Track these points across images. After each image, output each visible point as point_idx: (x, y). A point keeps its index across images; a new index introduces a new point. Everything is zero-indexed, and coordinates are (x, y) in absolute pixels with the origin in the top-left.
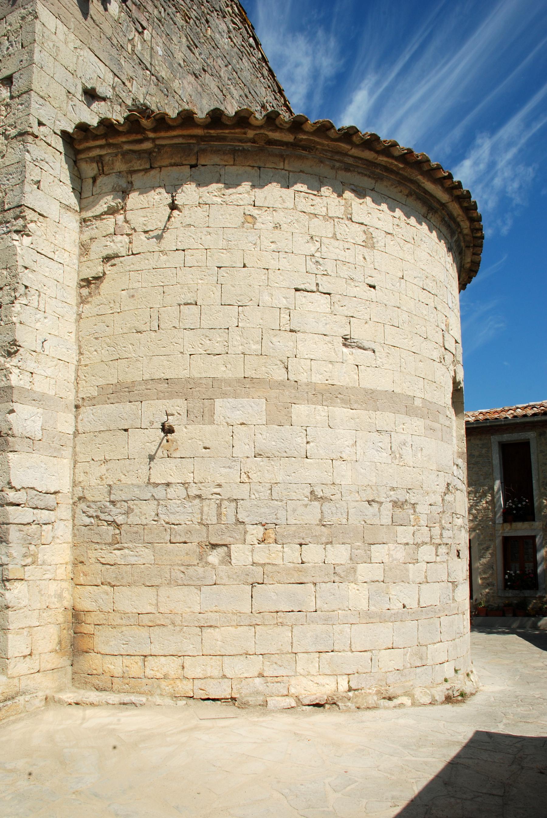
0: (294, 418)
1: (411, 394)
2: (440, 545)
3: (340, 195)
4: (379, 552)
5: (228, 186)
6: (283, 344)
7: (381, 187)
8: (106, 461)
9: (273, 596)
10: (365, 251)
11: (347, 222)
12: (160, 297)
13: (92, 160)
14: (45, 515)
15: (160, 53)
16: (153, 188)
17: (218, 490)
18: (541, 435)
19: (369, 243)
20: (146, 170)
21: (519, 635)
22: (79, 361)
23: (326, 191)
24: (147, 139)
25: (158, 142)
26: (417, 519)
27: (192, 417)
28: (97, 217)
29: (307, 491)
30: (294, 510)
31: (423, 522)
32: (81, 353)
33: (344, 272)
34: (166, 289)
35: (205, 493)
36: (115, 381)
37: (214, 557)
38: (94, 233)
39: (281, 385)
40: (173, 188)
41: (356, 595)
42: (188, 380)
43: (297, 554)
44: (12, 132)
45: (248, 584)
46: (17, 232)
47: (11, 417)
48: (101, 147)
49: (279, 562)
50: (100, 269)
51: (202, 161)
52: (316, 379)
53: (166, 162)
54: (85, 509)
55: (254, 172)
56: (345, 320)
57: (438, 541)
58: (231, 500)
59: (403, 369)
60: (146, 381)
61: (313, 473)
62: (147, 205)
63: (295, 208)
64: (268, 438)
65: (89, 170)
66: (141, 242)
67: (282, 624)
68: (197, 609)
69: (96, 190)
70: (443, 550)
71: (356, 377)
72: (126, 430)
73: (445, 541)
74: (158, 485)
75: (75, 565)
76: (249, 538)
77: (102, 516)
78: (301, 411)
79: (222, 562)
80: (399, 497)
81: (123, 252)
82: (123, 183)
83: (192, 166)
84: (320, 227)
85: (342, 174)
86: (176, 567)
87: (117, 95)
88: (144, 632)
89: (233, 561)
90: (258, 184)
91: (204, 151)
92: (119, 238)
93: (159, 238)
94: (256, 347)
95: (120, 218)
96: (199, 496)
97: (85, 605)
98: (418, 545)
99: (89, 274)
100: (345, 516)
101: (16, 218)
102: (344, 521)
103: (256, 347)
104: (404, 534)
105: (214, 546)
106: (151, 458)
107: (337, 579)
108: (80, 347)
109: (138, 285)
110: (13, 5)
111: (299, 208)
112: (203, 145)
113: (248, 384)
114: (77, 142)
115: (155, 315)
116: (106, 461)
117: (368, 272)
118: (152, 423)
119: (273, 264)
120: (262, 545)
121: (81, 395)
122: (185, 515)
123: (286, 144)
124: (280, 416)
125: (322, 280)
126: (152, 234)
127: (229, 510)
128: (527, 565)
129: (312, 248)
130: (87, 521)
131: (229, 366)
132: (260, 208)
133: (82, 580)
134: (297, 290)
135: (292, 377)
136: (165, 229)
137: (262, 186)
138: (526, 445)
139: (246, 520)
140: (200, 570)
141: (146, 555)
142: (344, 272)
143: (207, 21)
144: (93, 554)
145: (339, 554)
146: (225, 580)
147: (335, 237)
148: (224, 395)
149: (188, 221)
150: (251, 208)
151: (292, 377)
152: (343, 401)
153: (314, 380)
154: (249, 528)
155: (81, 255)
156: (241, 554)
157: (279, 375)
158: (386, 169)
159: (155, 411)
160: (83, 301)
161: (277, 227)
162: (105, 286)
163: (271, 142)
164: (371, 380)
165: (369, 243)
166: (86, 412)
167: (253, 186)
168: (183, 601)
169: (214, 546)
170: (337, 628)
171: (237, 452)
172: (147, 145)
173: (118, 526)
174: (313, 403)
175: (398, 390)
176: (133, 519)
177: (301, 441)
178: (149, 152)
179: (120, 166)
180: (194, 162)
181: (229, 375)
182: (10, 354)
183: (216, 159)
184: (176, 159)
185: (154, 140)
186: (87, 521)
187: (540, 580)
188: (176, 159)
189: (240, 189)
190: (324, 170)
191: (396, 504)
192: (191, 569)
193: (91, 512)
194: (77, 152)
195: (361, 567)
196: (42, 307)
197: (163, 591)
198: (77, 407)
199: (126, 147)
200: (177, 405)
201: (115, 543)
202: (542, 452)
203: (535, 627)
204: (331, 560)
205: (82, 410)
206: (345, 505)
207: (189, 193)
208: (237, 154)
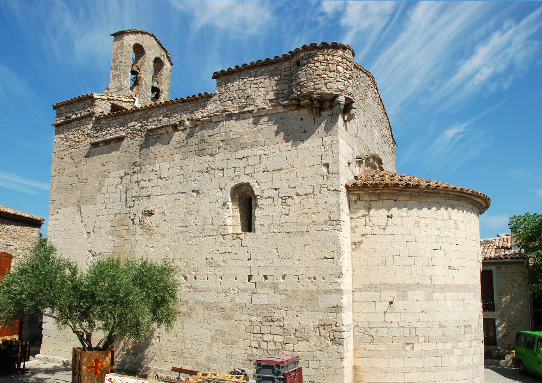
3: (447, 210)
4: (460, 344)
5: (409, 209)
7: (460, 203)
8: (367, 313)
9: (429, 361)
12: (385, 252)
13: (355, 194)
16: (380, 208)
17: (409, 324)
18: (498, 268)
19: (456, 228)
20: (377, 201)
21: (491, 369)
22: (353, 274)
23: (442, 209)
24: (379, 190)
26: (471, 331)
27: (399, 298)
28: (357, 218)
29: (438, 324)
31: (473, 332)
32: (353, 271)
35: (405, 325)
36: (369, 283)
37: (408, 348)
38: (357, 224)
40: (389, 209)
41: (454, 360)
42: (398, 285)
44: (332, 189)
46: (338, 230)
47: (341, 300)
48: (359, 190)
49: (430, 349)
50: (360, 239)
51: (399, 199)
52: (441, 283)
53: (385, 198)
54: (358, 330)
55: (418, 203)
56: (449, 260)
57: (477, 338)
60: (382, 284)
62: (378, 215)
63: (432, 217)
66: (377, 230)
67: (431, 371)
68: (403, 366)
75: (354, 350)
76: (420, 341)
77: (366, 333)
78: (436, 295)
79: (411, 350)
81: (370, 233)
82: (368, 205)
83: (395, 200)
84: (441, 224)
85: (448, 201)
88: (383, 375)
90: (420, 209)
91: (400, 195)
92: (368, 227)
93: (384, 229)
94: (421, 272)
95: (367, 219)
96: (403, 327)
97: (359, 364)
98: (472, 341)
99: (356, 240)
101: (337, 225)
103: (421, 272)
104: (468, 337)
105: (408, 344)
106: (385, 313)
108: (353, 269)
109: (377, 247)
110: (327, 133)
111: (434, 217)
112: (399, 193)
113: (418, 286)
115: (384, 260)
116: (367, 313)
121: (354, 287)
122: (398, 333)
124: (429, 298)
125: (442, 245)
126: (381, 227)
127: (413, 331)
128: (490, 332)
129: (438, 233)
130: (360, 334)
132: (420, 218)
133: (358, 355)
135: (433, 283)
136: (386, 226)
137: (421, 209)
138: (491, 271)
139: (419, 335)
140: (404, 352)
141: (383, 347)
144: (362, 347)
145: (448, 346)
147: (445, 227)
148: (411, 290)
149: (395, 223)
151: (433, 283)
154: (420, 337)
155: (351, 232)
156: (417, 347)
157: (429, 282)
158: (462, 197)
159: (388, 295)
160: (353, 250)
161: (427, 225)
162: (363, 246)
165: (456, 228)
166: (357, 294)
167: (418, 209)
168: (397, 363)
169: (408, 344)
170: (448, 372)
173: (372, 336)
175: (465, 284)
176: (378, 334)
177: (436, 306)
178: (379, 194)
179: (366, 198)
181: (412, 283)
182: (339, 277)
183: (404, 198)
184: (389, 198)
186: (360, 334)
187: (497, 341)
188: (389, 198)
189: (413, 210)
190: (442, 200)
193: (361, 331)
195: (455, 350)
197: (390, 360)
198: (353, 291)
199: (370, 192)
200: (394, 294)
201: (372, 342)
202: (498, 277)
203: (498, 365)
204: (446, 348)
205: (355, 293)
207: (394, 211)
208: (412, 196)
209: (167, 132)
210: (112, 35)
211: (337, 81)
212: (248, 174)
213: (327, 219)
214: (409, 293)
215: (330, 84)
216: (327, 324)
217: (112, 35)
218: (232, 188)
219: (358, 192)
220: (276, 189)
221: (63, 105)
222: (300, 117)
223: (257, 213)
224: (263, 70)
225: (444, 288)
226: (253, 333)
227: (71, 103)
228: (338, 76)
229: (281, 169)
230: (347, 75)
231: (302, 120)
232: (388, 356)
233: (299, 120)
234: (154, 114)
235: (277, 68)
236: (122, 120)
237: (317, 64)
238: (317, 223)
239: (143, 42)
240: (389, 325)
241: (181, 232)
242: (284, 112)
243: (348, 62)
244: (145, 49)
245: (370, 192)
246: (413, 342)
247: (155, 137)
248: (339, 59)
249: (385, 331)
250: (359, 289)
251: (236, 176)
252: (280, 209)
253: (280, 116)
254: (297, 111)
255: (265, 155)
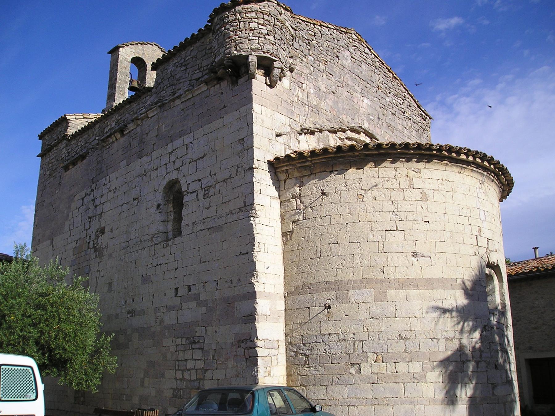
0: (388, 297)
1: (455, 277)
2: (480, 361)
6: (381, 260)
9: (382, 389)
10: (422, 203)
11: (410, 189)
14: (273, 352)
15: (312, 92)
19: (425, 198)
20: (309, 175)
24: (308, 161)
25: (313, 162)
30: (391, 345)
33: (411, 217)
34: (323, 236)
39: (381, 281)
43: (393, 367)
45: (369, 383)
48: (287, 166)
56: (412, 243)
57: (479, 359)
58: (359, 341)
59: (448, 264)
61: (400, 325)
64: (376, 309)
65: (283, 176)
69: (286, 187)
70: (482, 364)
71: (420, 273)
72: (309, 308)
73: (483, 359)
74: (325, 335)
78: (392, 293)
79: (356, 373)
80: (450, 335)
86: (335, 376)
87: (293, 129)
89: (362, 372)
100: (418, 347)
102: (418, 350)
107: (416, 381)
113: (366, 282)
114: (275, 166)
117: (424, 215)
118: (320, 304)
119: (373, 219)
120: (376, 364)
123: (376, 154)
124: (381, 297)
127: (358, 345)
131: (355, 274)
134: (386, 231)
139: (367, 351)
142: (411, 217)
143: (337, 57)
146: (359, 382)
148: (353, 288)
150: (360, 190)
152: (414, 286)
153: (397, 277)
157: (380, 276)
163: (367, 155)
164: (429, 273)
169: (353, 365)
170: (417, 407)
171: (361, 317)
172: (308, 163)
174: (398, 289)
177: (392, 309)
179: (296, 174)
180: (331, 170)
181: (355, 278)
185: (311, 161)
191: (447, 339)
192: (342, 376)
194: (275, 169)
196: (266, 251)
199: (298, 165)
200: (331, 294)
206: (417, 341)
209: (117, 139)
210: (108, 53)
211: (249, 40)
212: (177, 169)
213: (242, 205)
214: (351, 292)
215: (240, 45)
216: (243, 339)
217: (108, 53)
218: (165, 188)
219: (285, 168)
220: (199, 180)
221: (47, 133)
222: (221, 91)
223: (184, 212)
224: (192, 48)
225: (406, 284)
226: (179, 361)
227: (78, 135)
228: (251, 35)
229: (204, 156)
230: (264, 31)
231: (222, 93)
232: (326, 383)
233: (220, 94)
234: (109, 123)
235: (203, 43)
236: (87, 136)
237: (227, 27)
238: (233, 212)
239: (143, 54)
240: (326, 338)
241: (124, 249)
242: (208, 89)
243: (266, 17)
244: (146, 62)
245: (298, 165)
246: (359, 361)
247: (108, 147)
248: (254, 15)
249: (322, 347)
250: (291, 293)
251: (167, 173)
252: (204, 203)
253: (204, 95)
254: (218, 85)
255: (191, 143)
